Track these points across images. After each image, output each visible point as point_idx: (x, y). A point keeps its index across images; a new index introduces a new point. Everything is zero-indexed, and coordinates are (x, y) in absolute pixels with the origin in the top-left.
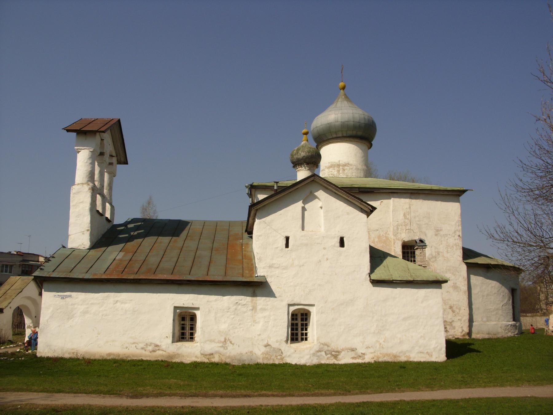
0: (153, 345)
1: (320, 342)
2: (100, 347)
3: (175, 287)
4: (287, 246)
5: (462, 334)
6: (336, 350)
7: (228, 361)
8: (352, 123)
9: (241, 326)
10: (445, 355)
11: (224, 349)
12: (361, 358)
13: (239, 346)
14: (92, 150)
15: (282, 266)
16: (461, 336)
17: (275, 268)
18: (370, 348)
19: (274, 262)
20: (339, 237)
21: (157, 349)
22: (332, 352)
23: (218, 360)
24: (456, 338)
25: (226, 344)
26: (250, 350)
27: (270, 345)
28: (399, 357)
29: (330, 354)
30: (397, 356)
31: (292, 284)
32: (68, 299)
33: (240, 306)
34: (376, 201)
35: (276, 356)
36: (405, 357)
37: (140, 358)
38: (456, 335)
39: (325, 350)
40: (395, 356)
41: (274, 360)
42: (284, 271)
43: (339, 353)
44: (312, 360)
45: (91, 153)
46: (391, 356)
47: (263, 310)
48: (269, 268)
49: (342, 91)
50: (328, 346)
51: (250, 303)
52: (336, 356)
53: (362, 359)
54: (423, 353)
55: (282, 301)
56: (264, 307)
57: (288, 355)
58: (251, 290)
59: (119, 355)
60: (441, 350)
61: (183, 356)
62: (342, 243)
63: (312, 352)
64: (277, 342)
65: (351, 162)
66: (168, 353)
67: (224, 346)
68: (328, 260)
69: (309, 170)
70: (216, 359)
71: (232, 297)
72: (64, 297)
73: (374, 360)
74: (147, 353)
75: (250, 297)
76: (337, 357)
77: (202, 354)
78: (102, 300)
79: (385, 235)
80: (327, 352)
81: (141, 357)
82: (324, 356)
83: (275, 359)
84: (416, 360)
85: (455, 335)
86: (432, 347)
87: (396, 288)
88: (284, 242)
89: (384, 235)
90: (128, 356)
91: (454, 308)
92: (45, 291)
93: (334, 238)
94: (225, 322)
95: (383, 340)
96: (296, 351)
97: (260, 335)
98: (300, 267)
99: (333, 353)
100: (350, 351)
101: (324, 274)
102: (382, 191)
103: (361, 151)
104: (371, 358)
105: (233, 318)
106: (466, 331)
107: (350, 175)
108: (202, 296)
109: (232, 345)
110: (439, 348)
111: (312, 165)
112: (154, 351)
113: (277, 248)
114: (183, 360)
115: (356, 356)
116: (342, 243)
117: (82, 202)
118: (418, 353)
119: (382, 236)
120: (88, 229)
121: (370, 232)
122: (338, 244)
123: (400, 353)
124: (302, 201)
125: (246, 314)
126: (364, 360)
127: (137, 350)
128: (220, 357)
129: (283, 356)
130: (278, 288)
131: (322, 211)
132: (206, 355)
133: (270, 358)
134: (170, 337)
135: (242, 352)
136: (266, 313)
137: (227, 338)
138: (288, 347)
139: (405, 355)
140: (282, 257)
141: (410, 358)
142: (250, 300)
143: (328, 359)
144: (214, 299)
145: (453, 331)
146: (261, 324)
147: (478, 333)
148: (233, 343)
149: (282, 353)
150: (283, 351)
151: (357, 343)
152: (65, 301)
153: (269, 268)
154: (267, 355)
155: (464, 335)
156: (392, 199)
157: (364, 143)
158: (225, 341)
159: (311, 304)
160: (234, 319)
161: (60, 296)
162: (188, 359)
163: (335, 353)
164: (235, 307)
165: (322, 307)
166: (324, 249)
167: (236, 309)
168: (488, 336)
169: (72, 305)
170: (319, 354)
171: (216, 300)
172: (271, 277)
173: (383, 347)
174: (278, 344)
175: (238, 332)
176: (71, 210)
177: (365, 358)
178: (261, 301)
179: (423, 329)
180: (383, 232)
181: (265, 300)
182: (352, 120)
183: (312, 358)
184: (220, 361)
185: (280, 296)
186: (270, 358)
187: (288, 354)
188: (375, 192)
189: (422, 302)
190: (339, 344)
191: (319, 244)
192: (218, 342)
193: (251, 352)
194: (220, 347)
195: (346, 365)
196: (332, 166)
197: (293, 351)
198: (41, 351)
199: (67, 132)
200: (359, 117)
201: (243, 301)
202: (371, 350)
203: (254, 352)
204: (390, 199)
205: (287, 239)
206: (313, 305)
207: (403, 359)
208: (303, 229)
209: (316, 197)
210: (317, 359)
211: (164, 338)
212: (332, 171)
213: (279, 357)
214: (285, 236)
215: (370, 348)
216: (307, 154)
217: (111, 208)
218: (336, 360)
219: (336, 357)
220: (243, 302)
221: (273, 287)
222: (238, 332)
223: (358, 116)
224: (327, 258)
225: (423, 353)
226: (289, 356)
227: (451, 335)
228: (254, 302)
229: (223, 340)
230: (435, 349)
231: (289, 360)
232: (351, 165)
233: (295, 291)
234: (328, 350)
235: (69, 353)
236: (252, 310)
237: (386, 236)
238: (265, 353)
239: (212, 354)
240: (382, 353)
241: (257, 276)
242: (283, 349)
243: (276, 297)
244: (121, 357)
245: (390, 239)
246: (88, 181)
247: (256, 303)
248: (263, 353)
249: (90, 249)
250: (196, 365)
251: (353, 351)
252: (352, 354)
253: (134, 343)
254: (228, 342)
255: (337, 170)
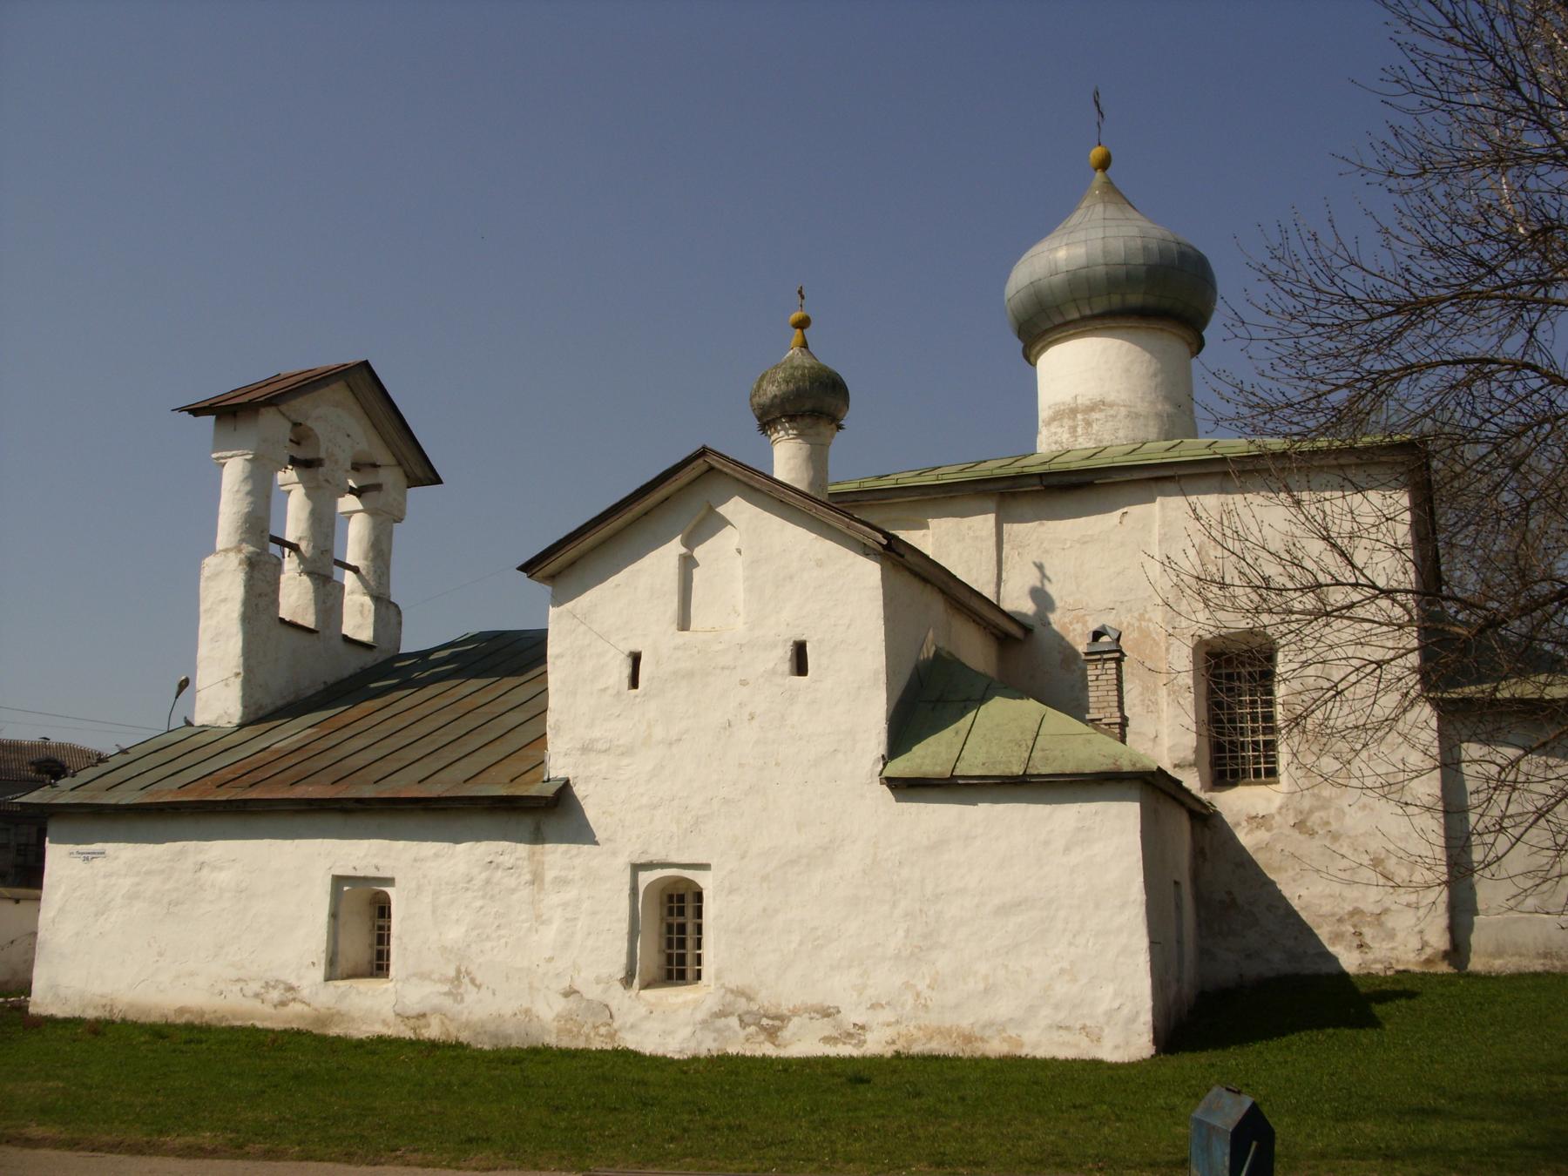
0: (281, 986)
1: (723, 986)
2: (161, 991)
3: (336, 821)
4: (634, 683)
5: (1424, 957)
6: (773, 1011)
7: (464, 1037)
8: (1101, 270)
9: (502, 932)
10: (1152, 1036)
11: (455, 1000)
12: (854, 1042)
13: (494, 994)
14: (251, 456)
15: (618, 746)
16: (1418, 963)
17: (600, 752)
18: (882, 1006)
19: (596, 733)
20: (791, 643)
21: (291, 997)
22: (761, 1018)
23: (438, 1035)
24: (1398, 972)
25: (459, 986)
26: (525, 1005)
27: (578, 992)
28: (982, 1039)
29: (754, 1024)
30: (976, 1039)
31: (644, 800)
32: (98, 862)
33: (499, 873)
34: (1105, 513)
35: (595, 1027)
36: (1004, 1040)
37: (249, 1023)
38: (1398, 961)
39: (740, 1012)
40: (968, 1039)
41: (588, 1037)
42: (625, 761)
43: (783, 1021)
44: (700, 1043)
45: (248, 466)
46: (954, 1036)
47: (562, 882)
48: (582, 754)
49: (1099, 174)
50: (750, 999)
51: (526, 863)
52: (772, 1031)
53: (855, 1046)
54: (1067, 1028)
55: (614, 854)
56: (563, 873)
57: (628, 1025)
58: (528, 822)
59: (202, 1014)
60: (1133, 1019)
61: (353, 1020)
62: (800, 660)
63: (699, 1016)
64: (598, 983)
65: (1111, 397)
66: (316, 1010)
67: (455, 992)
68: (753, 718)
69: (798, 436)
70: (433, 1031)
71: (479, 844)
72: (90, 856)
73: (895, 1047)
74: (268, 1009)
75: (526, 843)
76: (777, 1036)
77: (398, 1015)
78: (169, 861)
79: (1137, 624)
80: (747, 1019)
81: (253, 1019)
82: (735, 1031)
83: (592, 1035)
84: (1042, 1053)
85: (1393, 961)
86: (1102, 1008)
87: (975, 804)
88: (626, 671)
89: (1133, 625)
90: (223, 1017)
91: (1391, 864)
92: (51, 842)
93: (774, 646)
94: (458, 920)
95: (928, 981)
96: (651, 1012)
97: (551, 959)
98: (671, 744)
99: (765, 1021)
100: (818, 1016)
101: (741, 765)
102: (1118, 478)
103: (1148, 356)
104: (887, 1042)
105: (482, 908)
106: (1435, 945)
107: (1107, 439)
108: (401, 844)
109: (476, 990)
110: (1125, 1011)
111: (808, 420)
112: (283, 1004)
113: (605, 690)
114: (351, 1031)
115: (836, 1035)
116: (800, 660)
117: (224, 600)
118: (1050, 1027)
119: (1128, 628)
120: (238, 671)
121: (1087, 618)
122: (786, 666)
123: (984, 1027)
124: (680, 536)
125: (515, 897)
126: (862, 1046)
127: (244, 999)
128: (443, 1023)
129: (616, 1025)
130: (604, 813)
131: (740, 559)
132: (408, 1018)
133: (579, 1032)
134: (319, 964)
135: (502, 1012)
136: (570, 894)
137: (463, 969)
138: (630, 997)
139: (1004, 1035)
140: (619, 716)
141: (1022, 1045)
142: (524, 855)
143: (747, 1040)
144: (433, 851)
145: (1386, 945)
146: (555, 926)
147: (1499, 953)
148: (478, 982)
149: (611, 1016)
150: (614, 1010)
151: (839, 990)
152: (92, 867)
153: (582, 754)
154: (571, 1022)
155: (1428, 961)
156: (1159, 499)
157: (1162, 330)
158: (458, 978)
159: (700, 862)
160: (482, 912)
161: (82, 853)
162: (364, 1028)
163: (771, 1022)
164: (484, 875)
165: (732, 872)
166: (744, 683)
167: (488, 882)
168: (1543, 964)
169: (105, 876)
170: (721, 1022)
171: (436, 855)
172: (587, 780)
173: (925, 1006)
174: (601, 987)
175: (492, 949)
176: (203, 624)
177: (865, 1042)
178: (556, 855)
179: (1070, 944)
180: (1129, 616)
181: (566, 852)
182: (1101, 261)
183: (699, 1034)
184: (443, 1038)
185: (608, 840)
186: (579, 1032)
187: (631, 1020)
188: (1097, 482)
189: (1067, 850)
190: (782, 992)
191: (728, 668)
192: (440, 981)
193: (527, 1012)
194: (445, 994)
195: (806, 1063)
196: (1070, 412)
197: (643, 1011)
198: (38, 1000)
199: (196, 415)
200: (1125, 247)
201: (505, 858)
202: (887, 1015)
203: (534, 1010)
204: (1153, 501)
205: (636, 659)
206: (705, 867)
207: (996, 1047)
208: (684, 623)
209: (724, 522)
210: (715, 1040)
211: (308, 967)
212: (1055, 433)
213: (603, 1030)
214: (627, 652)
215: (882, 1006)
216: (783, 387)
217: (375, 610)
218: (773, 1043)
219: (772, 1034)
220: (507, 860)
221: (592, 813)
222: (492, 949)
223: (1122, 245)
224: (750, 714)
225: (1067, 1028)
226: (632, 1027)
227: (1381, 962)
228: (535, 859)
229: (452, 973)
230: (1109, 1014)
231: (631, 1041)
232: (1111, 405)
233: (651, 821)
234: (748, 1013)
235: (95, 1008)
236: (533, 883)
237: (1140, 628)
238: (562, 1017)
239: (424, 1015)
240: (923, 1026)
241: (549, 780)
242: (614, 1007)
243: (596, 843)
244: (207, 1017)
245: (1154, 636)
246: (242, 541)
247: (543, 863)
248: (558, 1017)
249: (241, 726)
250: (380, 1046)
251: (828, 1015)
252: (825, 1027)
253: (238, 980)
254: (466, 980)
255: (1070, 427)
